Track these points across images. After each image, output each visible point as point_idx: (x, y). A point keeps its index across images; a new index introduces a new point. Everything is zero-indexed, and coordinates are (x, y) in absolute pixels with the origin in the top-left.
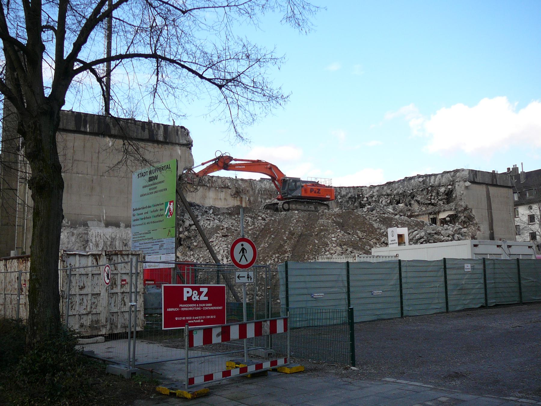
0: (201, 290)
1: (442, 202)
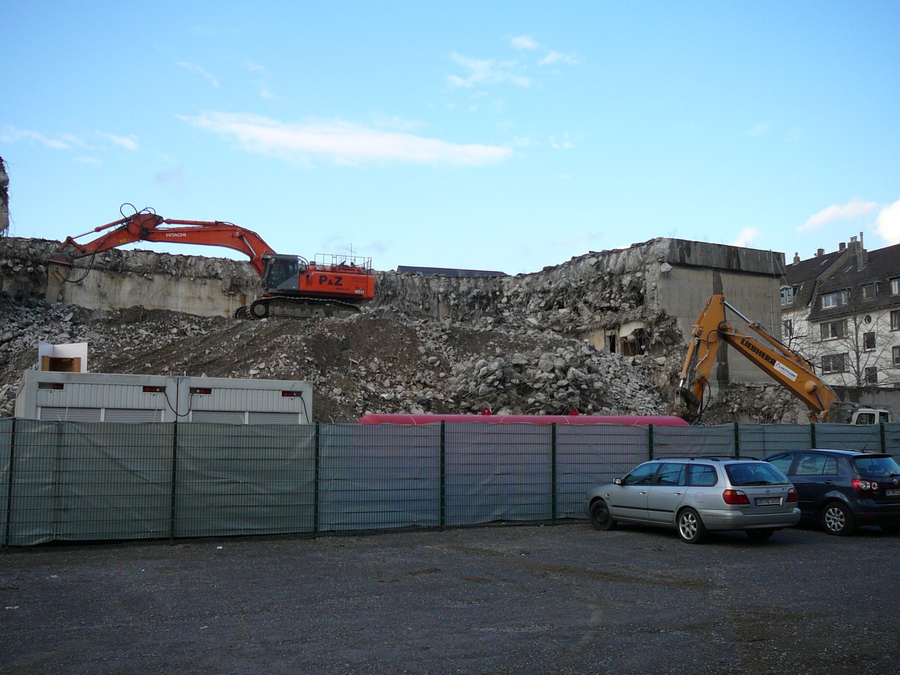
1: (628, 305)
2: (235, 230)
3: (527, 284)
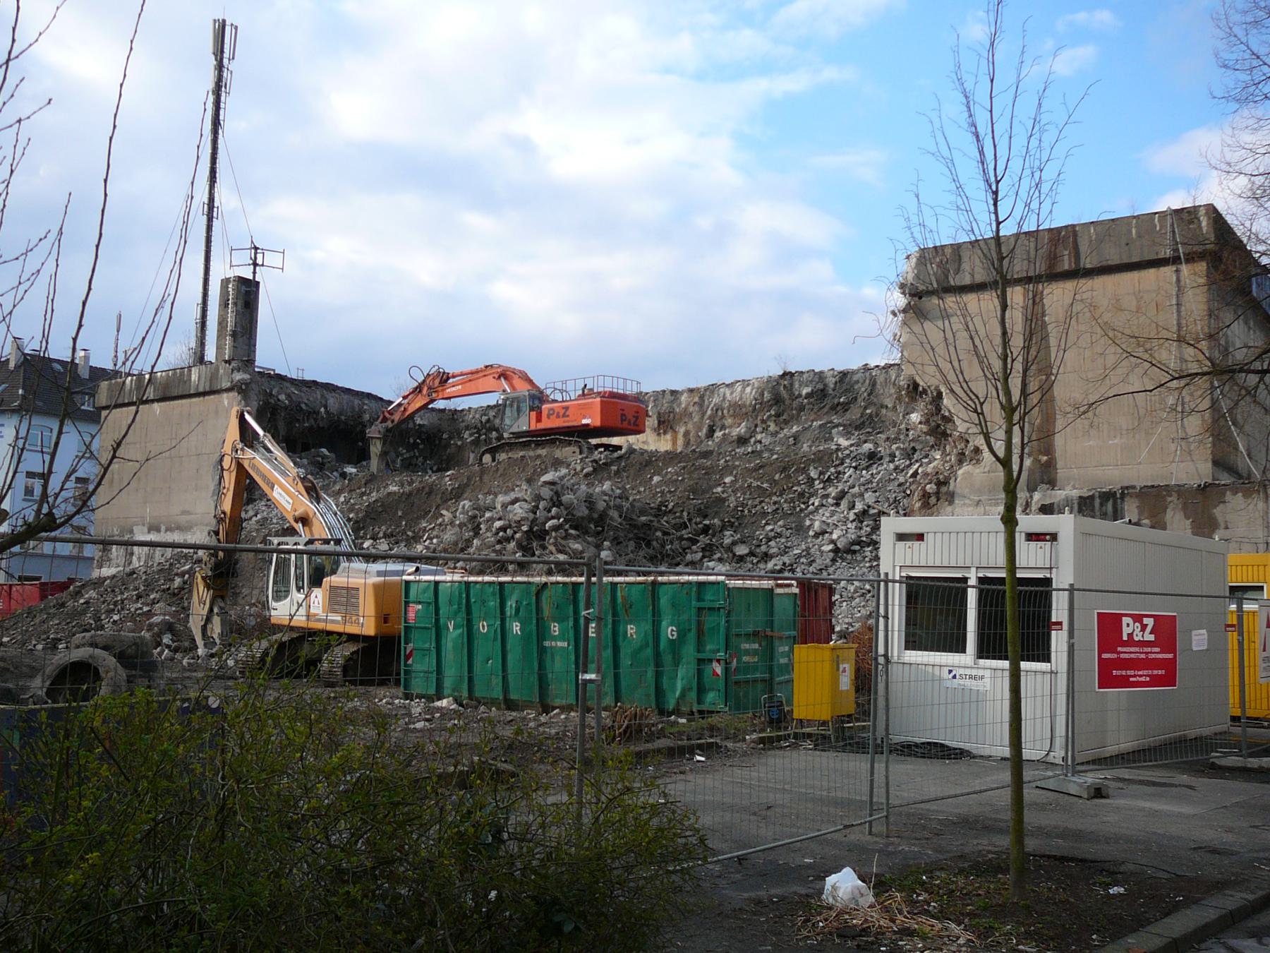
0: (1146, 621)
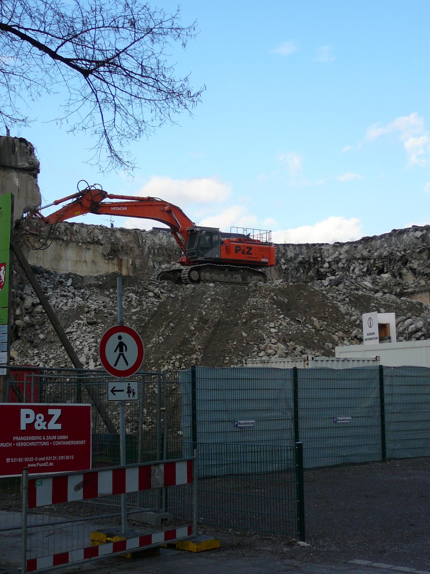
2: (164, 205)
3: (346, 252)
